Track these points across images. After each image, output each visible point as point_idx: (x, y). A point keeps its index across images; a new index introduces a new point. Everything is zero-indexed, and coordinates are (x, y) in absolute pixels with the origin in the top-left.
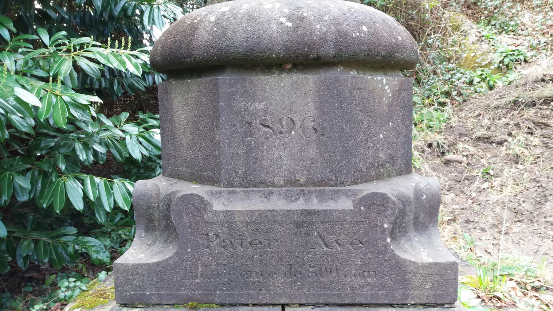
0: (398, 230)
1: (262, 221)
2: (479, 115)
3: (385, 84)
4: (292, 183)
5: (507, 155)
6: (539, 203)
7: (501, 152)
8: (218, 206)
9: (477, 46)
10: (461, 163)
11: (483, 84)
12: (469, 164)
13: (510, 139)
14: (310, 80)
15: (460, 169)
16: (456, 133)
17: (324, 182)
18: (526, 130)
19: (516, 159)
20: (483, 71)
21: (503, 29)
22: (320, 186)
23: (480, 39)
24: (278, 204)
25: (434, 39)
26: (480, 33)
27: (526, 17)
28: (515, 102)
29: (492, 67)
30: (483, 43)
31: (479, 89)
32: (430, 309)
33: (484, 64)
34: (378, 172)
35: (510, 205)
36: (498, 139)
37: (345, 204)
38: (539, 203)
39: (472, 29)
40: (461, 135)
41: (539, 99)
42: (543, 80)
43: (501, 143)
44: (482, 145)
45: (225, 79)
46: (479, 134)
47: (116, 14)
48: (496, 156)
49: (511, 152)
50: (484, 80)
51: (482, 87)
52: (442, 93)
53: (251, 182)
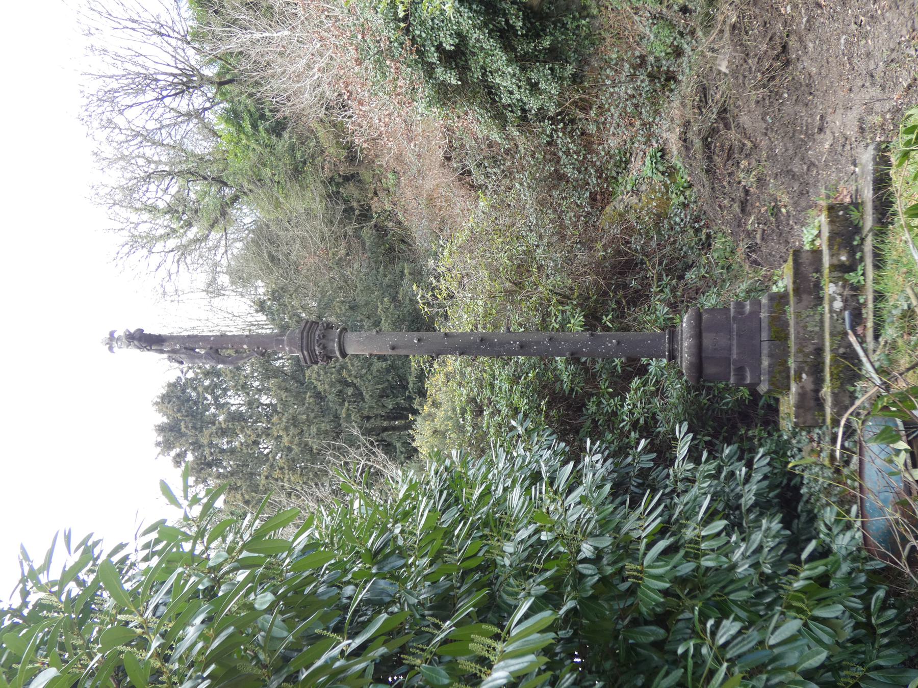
0: (742, 313)
1: (739, 346)
2: (720, 206)
3: (705, 316)
4: (730, 339)
5: (757, 188)
6: (793, 176)
7: (755, 193)
8: (735, 357)
9: (643, 198)
10: (764, 230)
11: (687, 193)
12: (765, 224)
13: (743, 183)
14: (704, 335)
15: (769, 231)
16: (737, 229)
17: (730, 332)
18: (734, 168)
19: (761, 181)
20: (672, 192)
21: (624, 164)
22: (822, 371)
23: (636, 192)
24: (735, 342)
25: (637, 243)
26: (628, 193)
27: (613, 143)
28: (707, 171)
29: (669, 182)
30: (640, 189)
31: (693, 199)
32: (53, 560)
33: (663, 190)
34: (728, 318)
35: (796, 199)
36: (743, 195)
37: (735, 326)
38: (793, 176)
39: (623, 199)
40: (739, 226)
41: (704, 152)
42: (685, 141)
43: (747, 192)
44: (749, 208)
45: (703, 355)
46: (738, 210)
47: (571, 632)
48: (758, 197)
49: (755, 185)
50: (682, 193)
51: (691, 196)
52: (696, 236)
53: (730, 349)
